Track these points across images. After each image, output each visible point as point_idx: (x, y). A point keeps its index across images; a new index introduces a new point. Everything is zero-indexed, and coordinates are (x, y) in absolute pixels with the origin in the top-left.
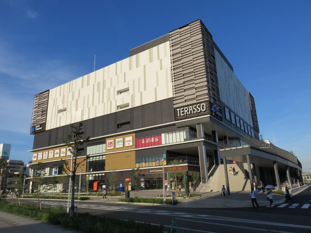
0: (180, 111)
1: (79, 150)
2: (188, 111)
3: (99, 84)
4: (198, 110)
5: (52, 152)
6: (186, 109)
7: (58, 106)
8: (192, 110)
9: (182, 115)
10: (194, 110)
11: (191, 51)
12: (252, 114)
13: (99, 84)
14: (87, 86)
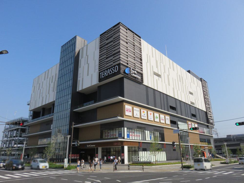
0: (102, 74)
1: (173, 123)
2: (107, 74)
3: (53, 77)
4: (113, 71)
5: (151, 114)
6: (106, 72)
7: (152, 66)
8: (109, 72)
9: (103, 77)
10: (111, 72)
11: (105, 66)
12: (205, 102)
13: (53, 77)
14: (94, 73)
